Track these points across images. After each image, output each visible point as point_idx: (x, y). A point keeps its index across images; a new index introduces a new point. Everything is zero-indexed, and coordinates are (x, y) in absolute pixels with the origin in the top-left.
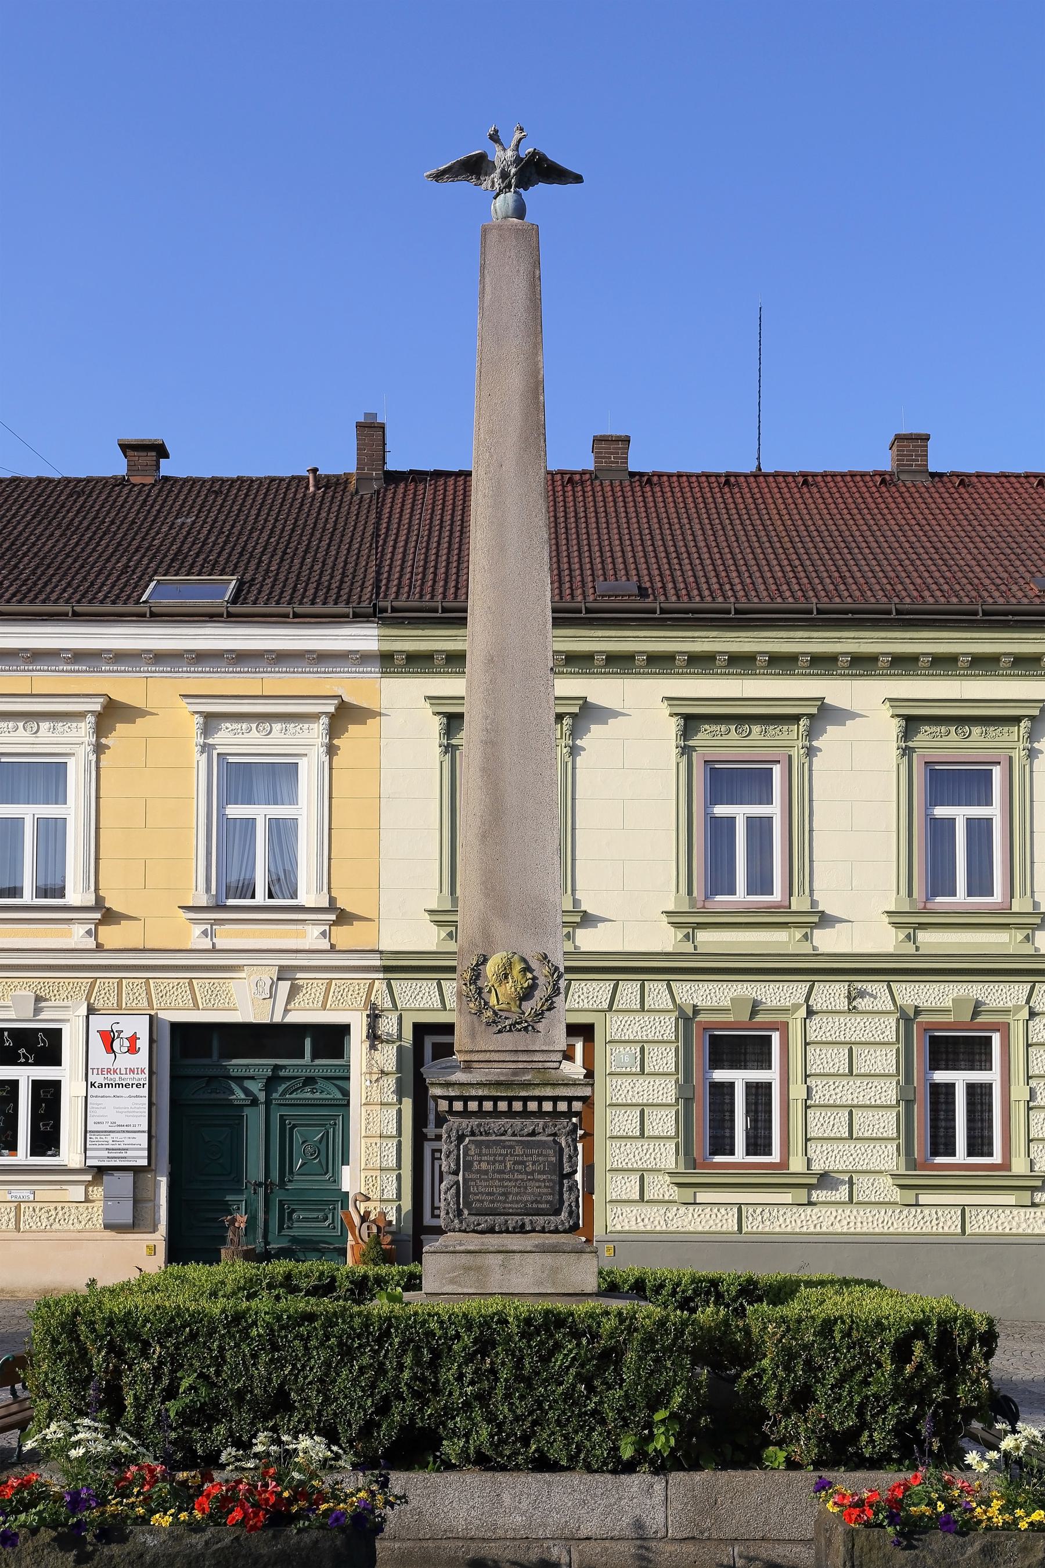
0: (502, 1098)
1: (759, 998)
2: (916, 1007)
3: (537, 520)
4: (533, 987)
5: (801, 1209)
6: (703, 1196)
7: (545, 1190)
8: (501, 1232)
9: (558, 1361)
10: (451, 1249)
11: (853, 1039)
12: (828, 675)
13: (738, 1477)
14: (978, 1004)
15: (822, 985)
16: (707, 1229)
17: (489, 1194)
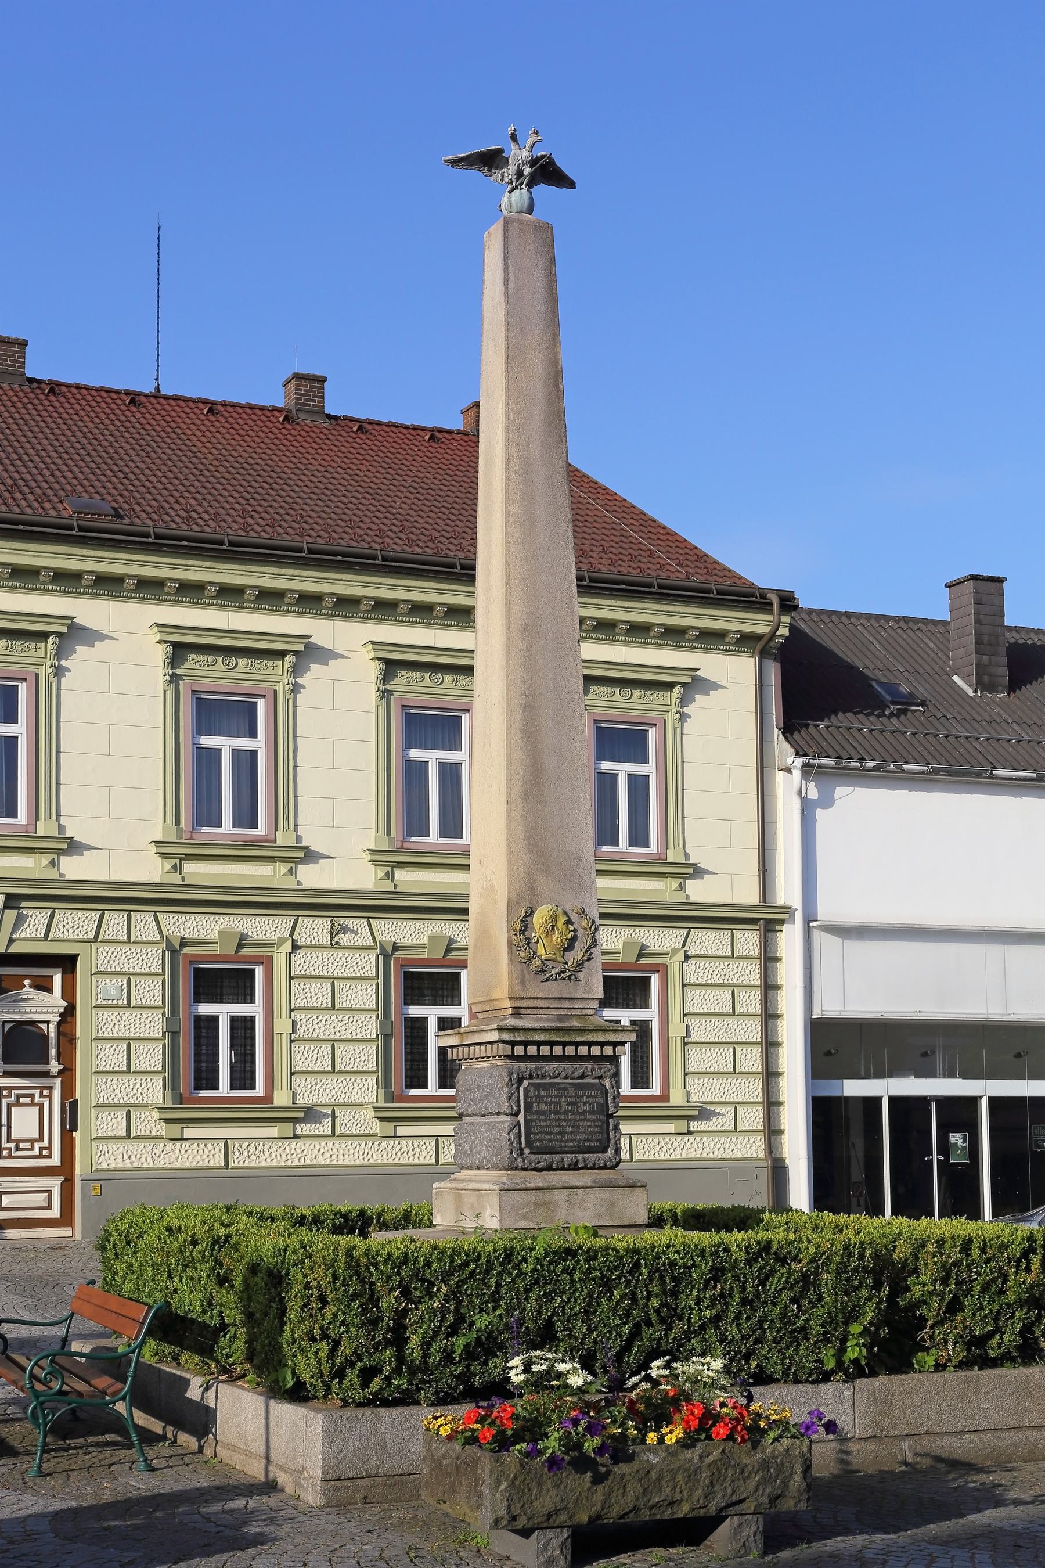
0: (558, 1043)
1: (246, 931)
2: (395, 943)
3: (561, 500)
4: (574, 939)
5: (286, 1143)
6: (190, 1132)
7: (594, 1129)
8: (556, 1170)
9: (773, 1284)
10: (523, 1186)
11: (335, 974)
12: (313, 614)
13: (897, 1380)
14: (643, 947)
15: (306, 920)
16: (194, 1164)
17: (547, 1133)
